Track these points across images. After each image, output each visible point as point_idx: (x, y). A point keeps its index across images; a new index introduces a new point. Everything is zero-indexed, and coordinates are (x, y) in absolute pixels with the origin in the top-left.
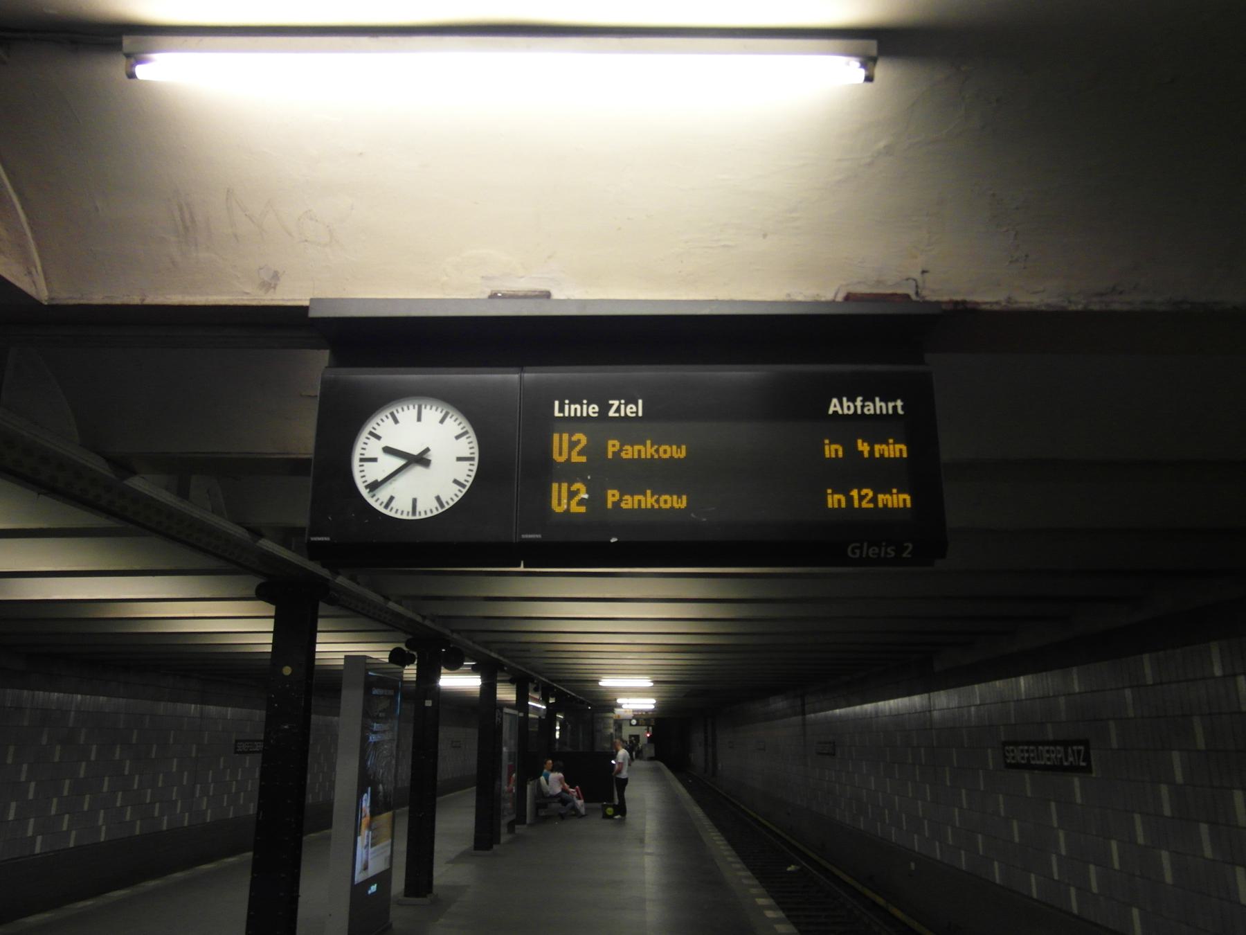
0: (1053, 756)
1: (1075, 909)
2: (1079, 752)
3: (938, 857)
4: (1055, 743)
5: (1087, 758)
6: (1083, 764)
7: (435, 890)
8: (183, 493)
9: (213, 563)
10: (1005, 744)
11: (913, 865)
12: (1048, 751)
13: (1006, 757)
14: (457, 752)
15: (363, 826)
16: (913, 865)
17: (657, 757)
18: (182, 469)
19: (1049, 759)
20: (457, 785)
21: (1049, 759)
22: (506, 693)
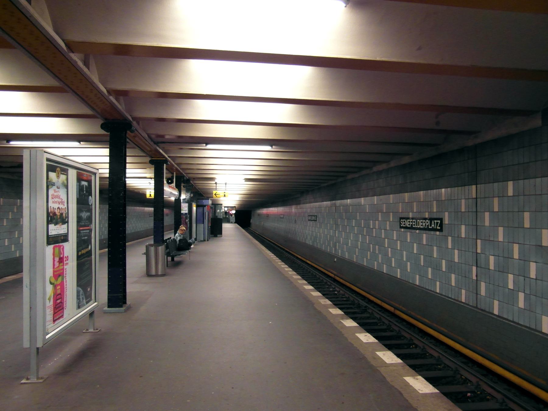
0: (424, 224)
1: (496, 312)
2: (437, 223)
4: (412, 219)
5: (441, 225)
6: (438, 228)
7: (128, 302)
10: (401, 218)
11: (336, 260)
12: (422, 222)
13: (400, 224)
14: (138, 219)
15: (478, 141)
16: (336, 260)
17: (235, 223)
19: (422, 225)
20: (139, 236)
21: (422, 225)
22: (140, 178)
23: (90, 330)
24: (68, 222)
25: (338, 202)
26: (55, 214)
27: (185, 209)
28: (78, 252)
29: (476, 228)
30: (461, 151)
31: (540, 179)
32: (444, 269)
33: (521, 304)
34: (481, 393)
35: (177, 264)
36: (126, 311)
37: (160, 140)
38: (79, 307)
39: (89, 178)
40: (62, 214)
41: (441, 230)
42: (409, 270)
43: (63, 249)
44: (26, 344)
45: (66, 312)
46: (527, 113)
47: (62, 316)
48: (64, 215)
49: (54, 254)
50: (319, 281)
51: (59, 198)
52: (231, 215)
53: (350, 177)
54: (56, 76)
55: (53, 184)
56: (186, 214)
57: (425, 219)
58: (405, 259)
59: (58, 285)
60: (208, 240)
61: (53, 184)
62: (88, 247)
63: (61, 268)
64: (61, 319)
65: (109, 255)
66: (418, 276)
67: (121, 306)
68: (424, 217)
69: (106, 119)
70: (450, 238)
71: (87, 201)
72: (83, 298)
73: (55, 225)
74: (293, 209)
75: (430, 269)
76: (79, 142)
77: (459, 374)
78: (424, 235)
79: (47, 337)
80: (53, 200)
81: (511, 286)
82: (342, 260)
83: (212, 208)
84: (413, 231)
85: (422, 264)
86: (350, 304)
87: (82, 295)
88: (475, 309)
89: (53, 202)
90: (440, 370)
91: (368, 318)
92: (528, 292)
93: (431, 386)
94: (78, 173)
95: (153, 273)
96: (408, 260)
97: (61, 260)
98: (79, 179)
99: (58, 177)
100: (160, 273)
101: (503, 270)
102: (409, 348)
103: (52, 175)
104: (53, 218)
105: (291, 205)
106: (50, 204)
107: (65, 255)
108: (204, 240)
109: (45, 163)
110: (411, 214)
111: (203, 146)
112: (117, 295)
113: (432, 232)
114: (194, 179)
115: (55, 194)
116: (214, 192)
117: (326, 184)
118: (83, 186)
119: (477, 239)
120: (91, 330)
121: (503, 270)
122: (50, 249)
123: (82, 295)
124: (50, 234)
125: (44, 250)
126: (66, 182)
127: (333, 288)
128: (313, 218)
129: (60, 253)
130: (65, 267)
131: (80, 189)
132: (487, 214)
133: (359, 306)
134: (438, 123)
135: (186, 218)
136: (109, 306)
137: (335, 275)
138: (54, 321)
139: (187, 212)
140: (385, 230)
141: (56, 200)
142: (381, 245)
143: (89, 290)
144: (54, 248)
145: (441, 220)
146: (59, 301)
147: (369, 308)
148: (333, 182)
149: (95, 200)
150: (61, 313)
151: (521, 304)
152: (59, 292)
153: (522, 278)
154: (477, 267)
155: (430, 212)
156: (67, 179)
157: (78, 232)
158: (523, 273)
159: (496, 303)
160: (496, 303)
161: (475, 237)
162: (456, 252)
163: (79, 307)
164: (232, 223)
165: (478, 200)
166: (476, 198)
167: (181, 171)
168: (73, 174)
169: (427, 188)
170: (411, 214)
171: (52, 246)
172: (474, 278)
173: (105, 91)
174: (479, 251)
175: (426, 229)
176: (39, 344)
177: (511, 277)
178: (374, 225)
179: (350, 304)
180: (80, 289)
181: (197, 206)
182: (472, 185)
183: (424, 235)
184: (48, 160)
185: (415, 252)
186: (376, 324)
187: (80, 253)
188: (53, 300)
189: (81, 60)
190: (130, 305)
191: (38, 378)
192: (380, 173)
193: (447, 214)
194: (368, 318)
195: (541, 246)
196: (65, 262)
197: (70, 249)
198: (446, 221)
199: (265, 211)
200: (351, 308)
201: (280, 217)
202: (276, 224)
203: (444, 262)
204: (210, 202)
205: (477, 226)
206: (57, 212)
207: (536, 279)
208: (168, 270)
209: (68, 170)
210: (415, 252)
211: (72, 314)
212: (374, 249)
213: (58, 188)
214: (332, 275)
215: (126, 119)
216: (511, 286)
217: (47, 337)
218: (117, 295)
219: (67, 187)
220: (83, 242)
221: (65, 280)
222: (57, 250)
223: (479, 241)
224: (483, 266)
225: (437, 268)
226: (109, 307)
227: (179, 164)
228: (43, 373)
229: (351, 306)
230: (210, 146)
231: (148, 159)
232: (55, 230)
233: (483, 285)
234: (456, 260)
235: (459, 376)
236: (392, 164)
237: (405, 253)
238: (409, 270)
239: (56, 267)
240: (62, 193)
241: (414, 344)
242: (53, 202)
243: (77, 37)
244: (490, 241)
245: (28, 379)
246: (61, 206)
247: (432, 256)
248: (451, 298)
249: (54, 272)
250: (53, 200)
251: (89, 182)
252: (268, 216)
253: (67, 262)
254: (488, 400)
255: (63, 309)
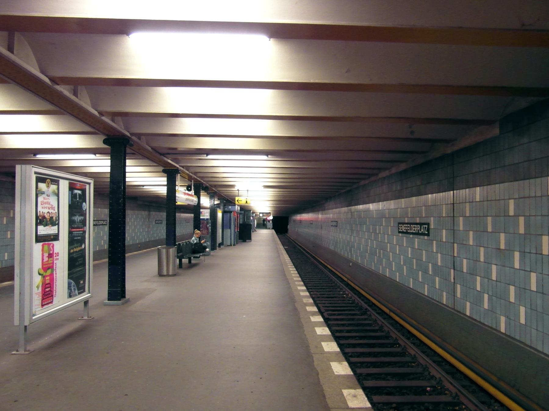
3: (426, 294)
4: (407, 224)
5: (428, 230)
6: (426, 232)
8: (113, 120)
9: (88, 129)
10: (399, 223)
15: (456, 148)
17: (273, 228)
18: (76, 83)
23: (85, 318)
24: (58, 224)
25: (353, 208)
26: (44, 217)
27: (205, 215)
28: (69, 250)
29: (453, 231)
30: (443, 158)
31: (498, 185)
32: (430, 273)
33: (486, 306)
34: (441, 388)
35: (191, 266)
36: (123, 304)
37: (175, 153)
38: (70, 296)
39: (84, 187)
40: (52, 218)
41: (428, 235)
42: (405, 274)
43: (53, 246)
44: (16, 322)
45: (55, 300)
46: (489, 123)
47: (52, 302)
48: (54, 218)
49: (43, 250)
50: (333, 284)
51: (50, 204)
52: (269, 221)
53: (362, 183)
54: (52, 103)
55: (43, 193)
56: (207, 219)
57: (417, 224)
58: (402, 264)
59: (47, 276)
60: (234, 245)
61: (43, 193)
62: (81, 246)
63: (50, 262)
64: (50, 305)
65: (109, 253)
66: (411, 279)
67: (119, 300)
68: (415, 222)
69: (107, 135)
70: (434, 242)
71: (81, 208)
72: (75, 289)
73: (44, 226)
74: (320, 216)
75: (420, 273)
76: (95, 154)
77: (428, 371)
78: (416, 239)
79: (34, 318)
80: (43, 206)
81: (478, 288)
82: (356, 264)
83: (240, 214)
84: (408, 235)
85: (415, 268)
86: (354, 307)
87: (74, 286)
88: (453, 311)
89: (42, 208)
90: (412, 367)
91: (365, 319)
92: (490, 293)
93: (350, 369)
94: (70, 184)
95: (165, 273)
96: (404, 264)
97: (51, 256)
98: (72, 187)
99: (48, 187)
100: (170, 273)
101: (473, 273)
102: (393, 347)
103: (42, 186)
104: (41, 220)
105: (318, 211)
106: (40, 209)
107: (56, 251)
108: (231, 245)
109: (34, 177)
110: (406, 219)
111: (204, 157)
112: (117, 290)
113: (422, 237)
114: (215, 186)
115: (45, 201)
116: (237, 198)
117: (344, 191)
118: (76, 194)
119: (454, 243)
120: (86, 318)
121: (473, 273)
122: (38, 248)
123: (74, 286)
124: (39, 234)
125: (31, 248)
126: (56, 191)
127: (344, 292)
128: (335, 224)
129: (49, 250)
130: (55, 262)
131: (73, 197)
132: (461, 219)
133: (361, 308)
134: (412, 133)
135: (208, 223)
136: (109, 300)
137: (348, 279)
138: (43, 306)
139: (208, 217)
140: (388, 235)
141: (46, 206)
142: (385, 250)
143: (82, 282)
144: (43, 246)
145: (428, 224)
146: (47, 290)
147: (369, 311)
148: (348, 188)
149: (89, 206)
150: (50, 300)
151: (486, 306)
152: (48, 282)
153: (486, 280)
154: (454, 269)
155: (421, 217)
156: (58, 189)
157: (70, 233)
158: (487, 276)
159: (468, 304)
160: (468, 304)
161: (452, 241)
162: (439, 255)
163: (70, 296)
164: (269, 228)
165: (455, 205)
166: (453, 204)
167: (198, 179)
168: (64, 186)
169: (419, 194)
170: (406, 219)
171: (41, 244)
172: (452, 281)
173: (96, 113)
174: (455, 255)
175: (417, 234)
176: (27, 323)
177: (478, 278)
178: (380, 230)
179: (354, 307)
180: (72, 281)
181: (224, 212)
182: (450, 191)
183: (416, 239)
184: (36, 173)
185: (410, 256)
186: (370, 325)
187: (72, 251)
188: (46, 289)
189: (70, 92)
190: (129, 299)
191: (25, 351)
192: (384, 178)
193: (432, 219)
194: (365, 319)
195: (500, 249)
196: (55, 258)
197: (61, 247)
198: (432, 226)
199: (299, 217)
200: (353, 310)
201: (311, 223)
202: (307, 230)
203: (430, 265)
204: (237, 208)
205: (454, 230)
206: (47, 216)
207: (496, 281)
208: (180, 271)
209: (59, 181)
210: (410, 256)
211: (62, 300)
212: (380, 253)
213: (48, 196)
214: (346, 279)
215: (124, 135)
216: (478, 288)
217: (34, 318)
218: (117, 290)
219: (58, 195)
220: (75, 241)
221: (54, 273)
222: (46, 247)
223: (455, 245)
224: (458, 269)
225: (425, 272)
226: (109, 300)
227: (195, 173)
228: (32, 347)
229: (354, 308)
230: (210, 157)
231: (161, 169)
232: (43, 230)
233: (459, 287)
234: (439, 264)
235: (426, 373)
236: (394, 171)
237: (402, 257)
238: (405, 274)
239: (44, 261)
240: (53, 201)
241: (398, 344)
242: (42, 208)
243: (58, 73)
244: (463, 245)
245: (17, 351)
246: (50, 211)
247: (421, 260)
248: (435, 300)
249: (43, 264)
250: (43, 206)
251: (84, 191)
252: (301, 221)
253: (57, 257)
254: (446, 394)
255: (52, 296)
